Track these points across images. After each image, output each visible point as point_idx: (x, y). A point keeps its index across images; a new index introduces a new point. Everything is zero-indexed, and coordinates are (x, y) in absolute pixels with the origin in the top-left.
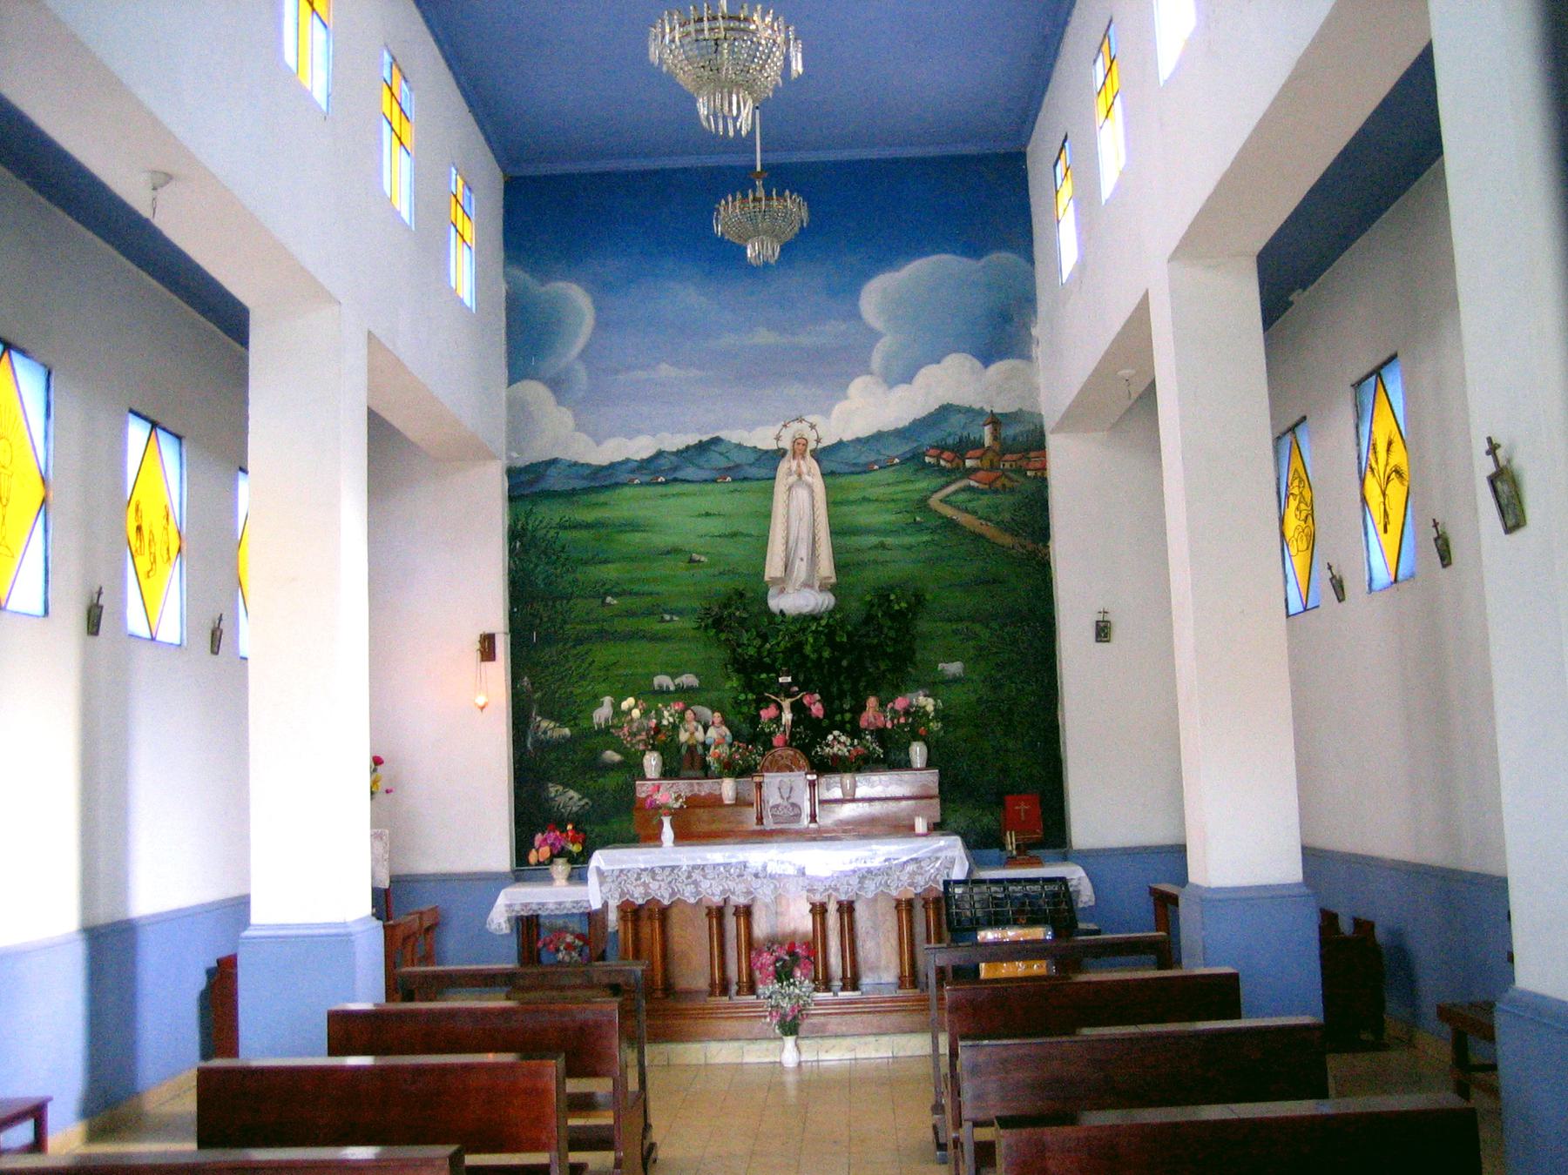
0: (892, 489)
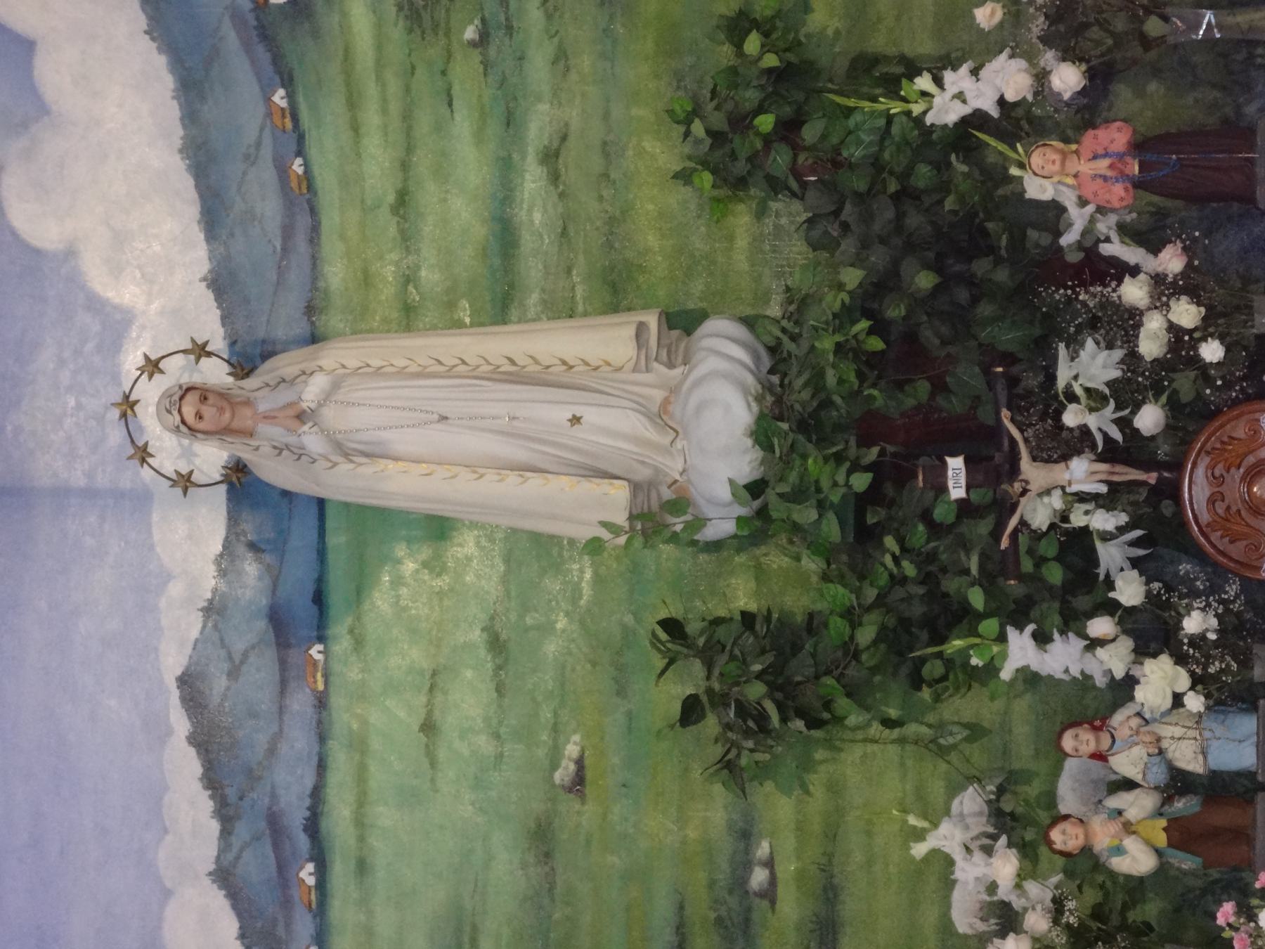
0: (372, 117)
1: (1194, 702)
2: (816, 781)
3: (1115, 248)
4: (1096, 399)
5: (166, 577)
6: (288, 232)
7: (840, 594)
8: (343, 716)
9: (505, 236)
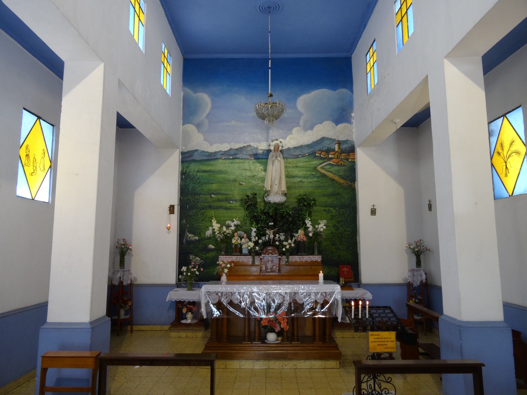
0: (305, 164)
1: (249, 248)
2: (241, 208)
3: (294, 239)
4: (279, 237)
5: (260, 143)
6: (294, 155)
7: (259, 211)
8: (247, 161)
9: (294, 177)
